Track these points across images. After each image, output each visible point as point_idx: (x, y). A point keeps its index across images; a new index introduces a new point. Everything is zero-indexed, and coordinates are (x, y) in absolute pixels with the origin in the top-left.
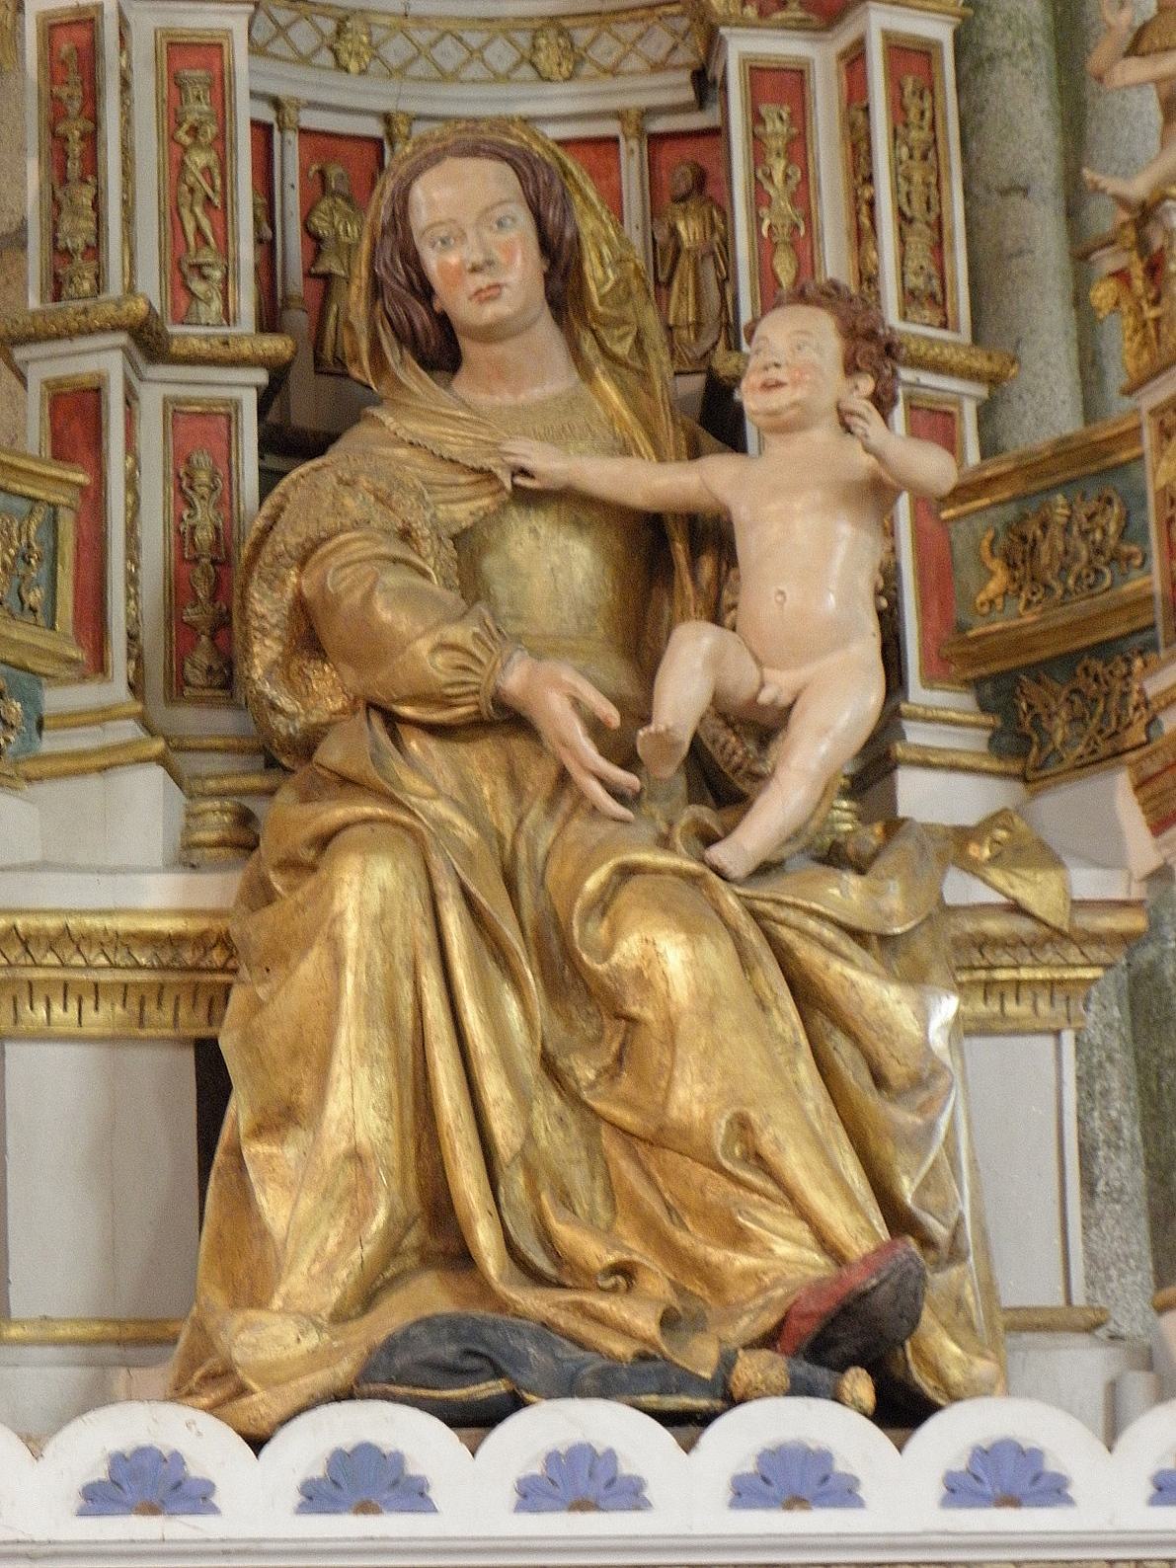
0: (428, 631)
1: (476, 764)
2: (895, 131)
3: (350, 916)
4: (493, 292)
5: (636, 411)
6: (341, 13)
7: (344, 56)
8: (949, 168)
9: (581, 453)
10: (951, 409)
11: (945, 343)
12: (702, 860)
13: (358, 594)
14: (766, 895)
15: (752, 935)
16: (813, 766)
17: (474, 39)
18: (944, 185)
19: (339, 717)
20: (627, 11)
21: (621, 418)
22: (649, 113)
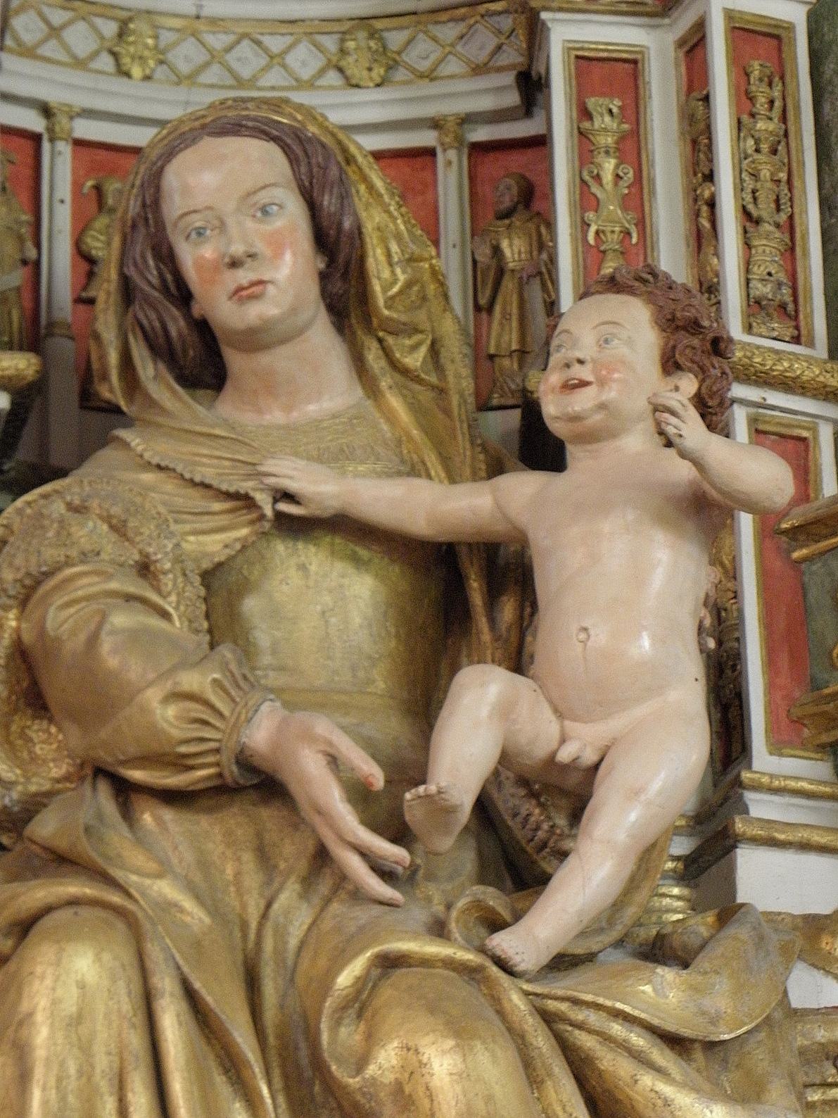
0: (162, 676)
1: (219, 838)
2: (739, 122)
3: (40, 1017)
4: (255, 289)
5: (428, 431)
6: (125, 14)
7: (126, 60)
8: (802, 164)
9: (357, 475)
10: (805, 434)
11: (797, 357)
12: (482, 950)
13: (82, 637)
14: (560, 993)
15: (541, 1041)
16: (621, 837)
17: (275, 44)
18: (796, 183)
19: (60, 786)
20: (446, 9)
21: (410, 438)
22: (468, 120)
